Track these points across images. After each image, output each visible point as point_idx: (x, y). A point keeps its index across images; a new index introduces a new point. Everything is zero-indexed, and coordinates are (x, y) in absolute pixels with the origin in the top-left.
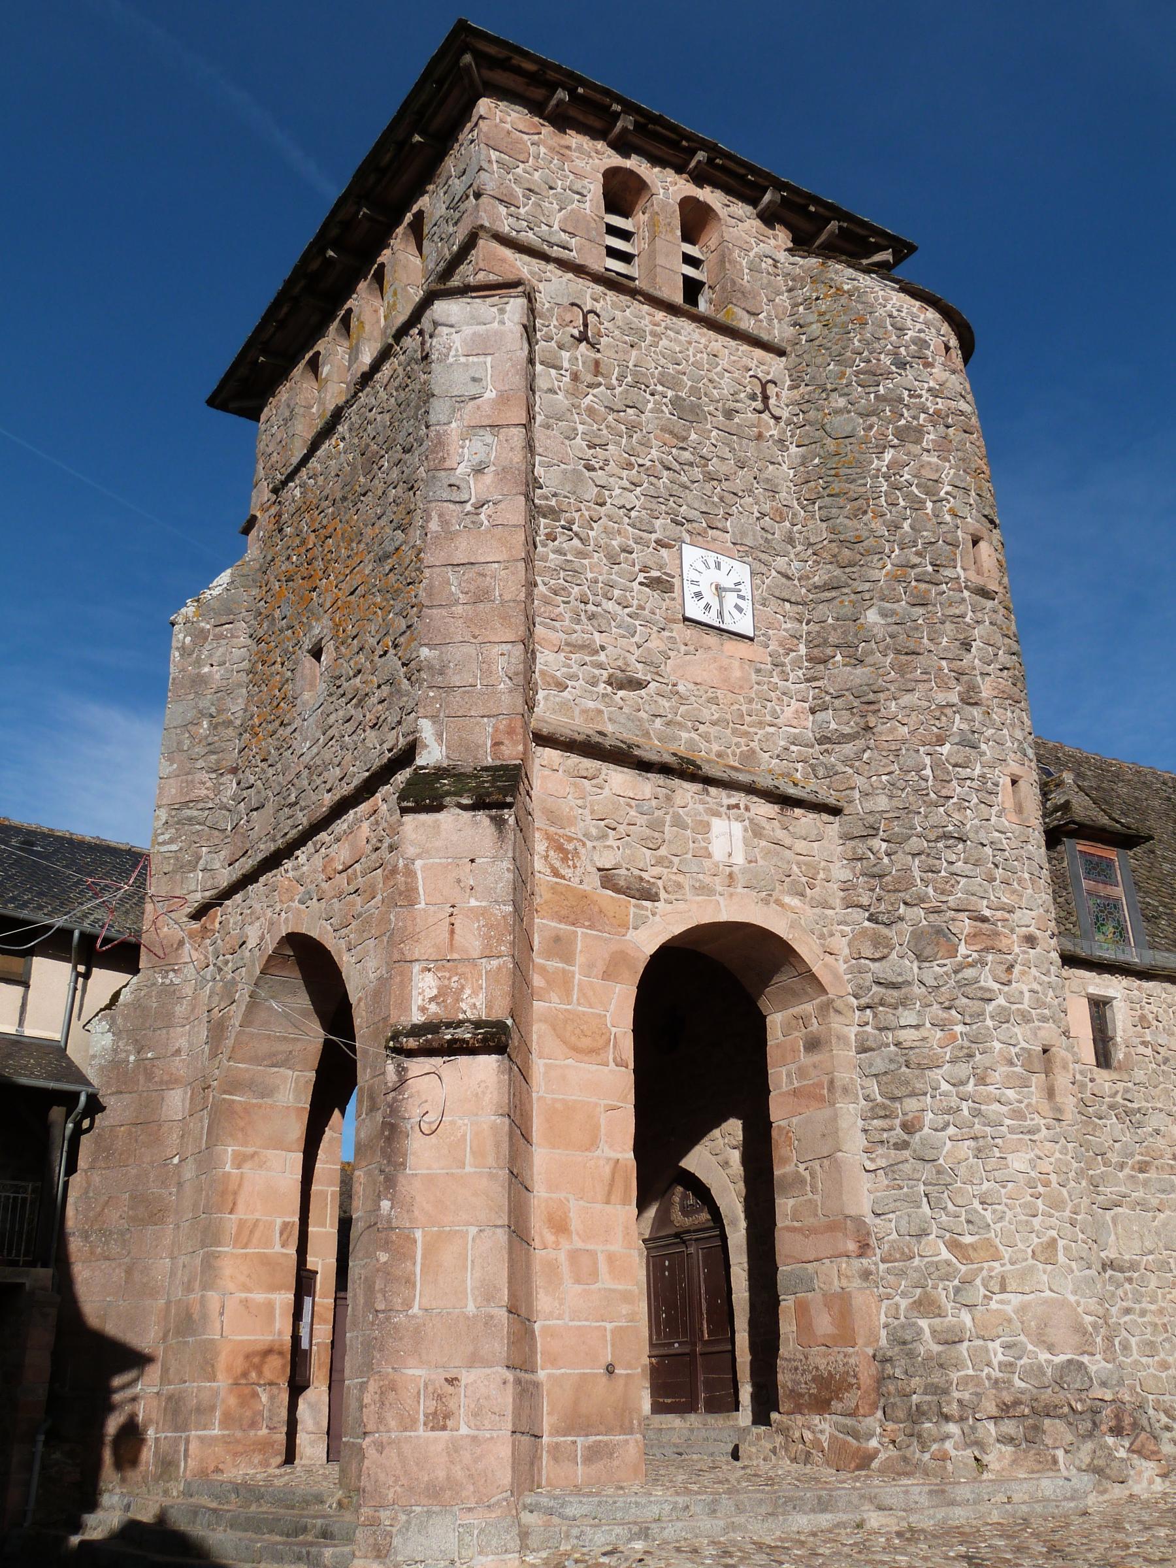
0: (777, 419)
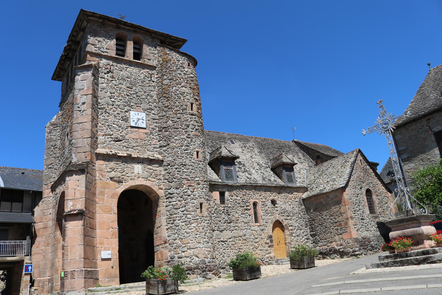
0: (154, 82)
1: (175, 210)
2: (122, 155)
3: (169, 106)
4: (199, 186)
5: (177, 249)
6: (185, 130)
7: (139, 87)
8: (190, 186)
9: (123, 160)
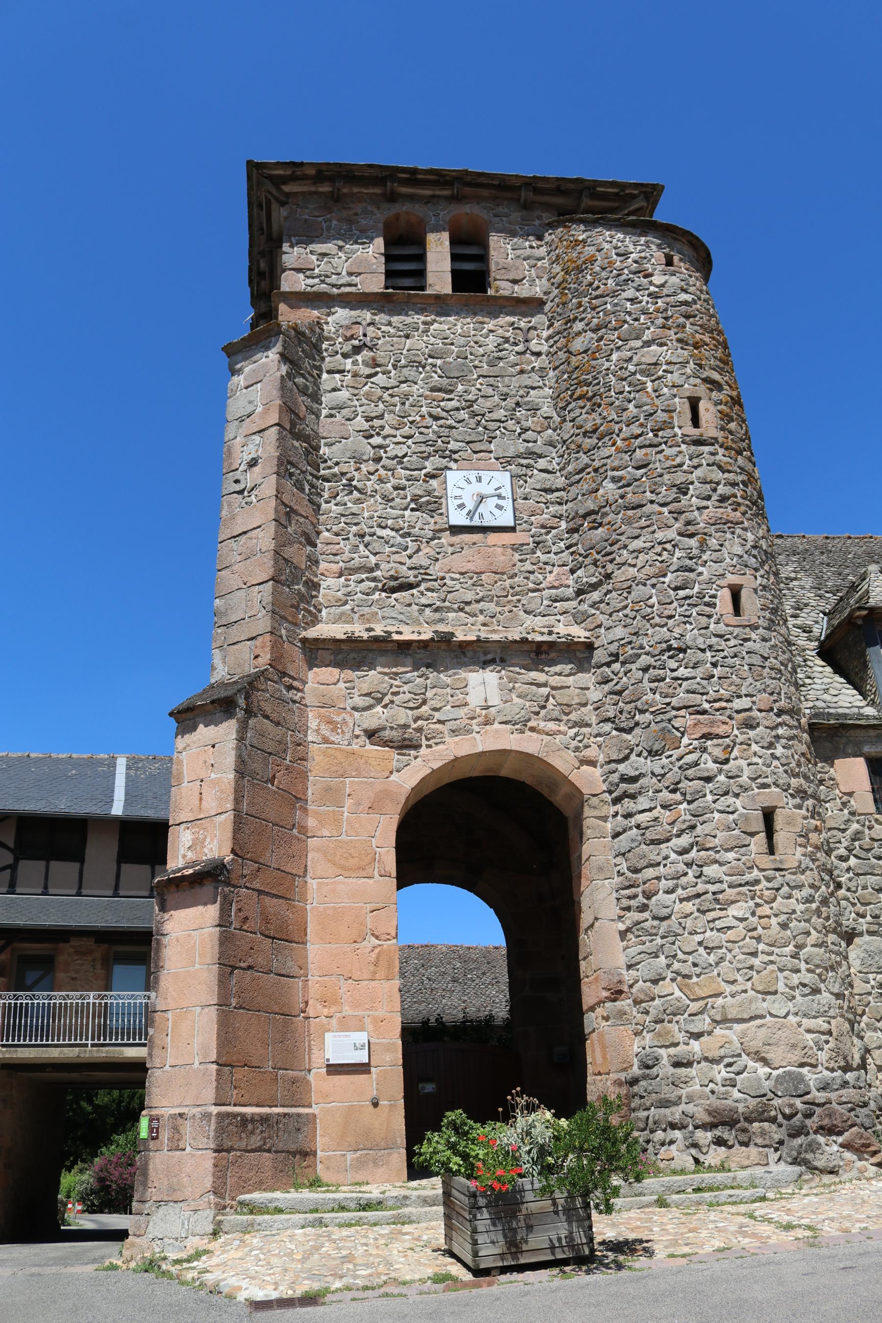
0: (538, 354)
2: (415, 637)
3: (602, 428)
4: (752, 733)
5: (666, 1023)
6: (670, 507)
7: (480, 380)
8: (707, 736)
9: (418, 656)
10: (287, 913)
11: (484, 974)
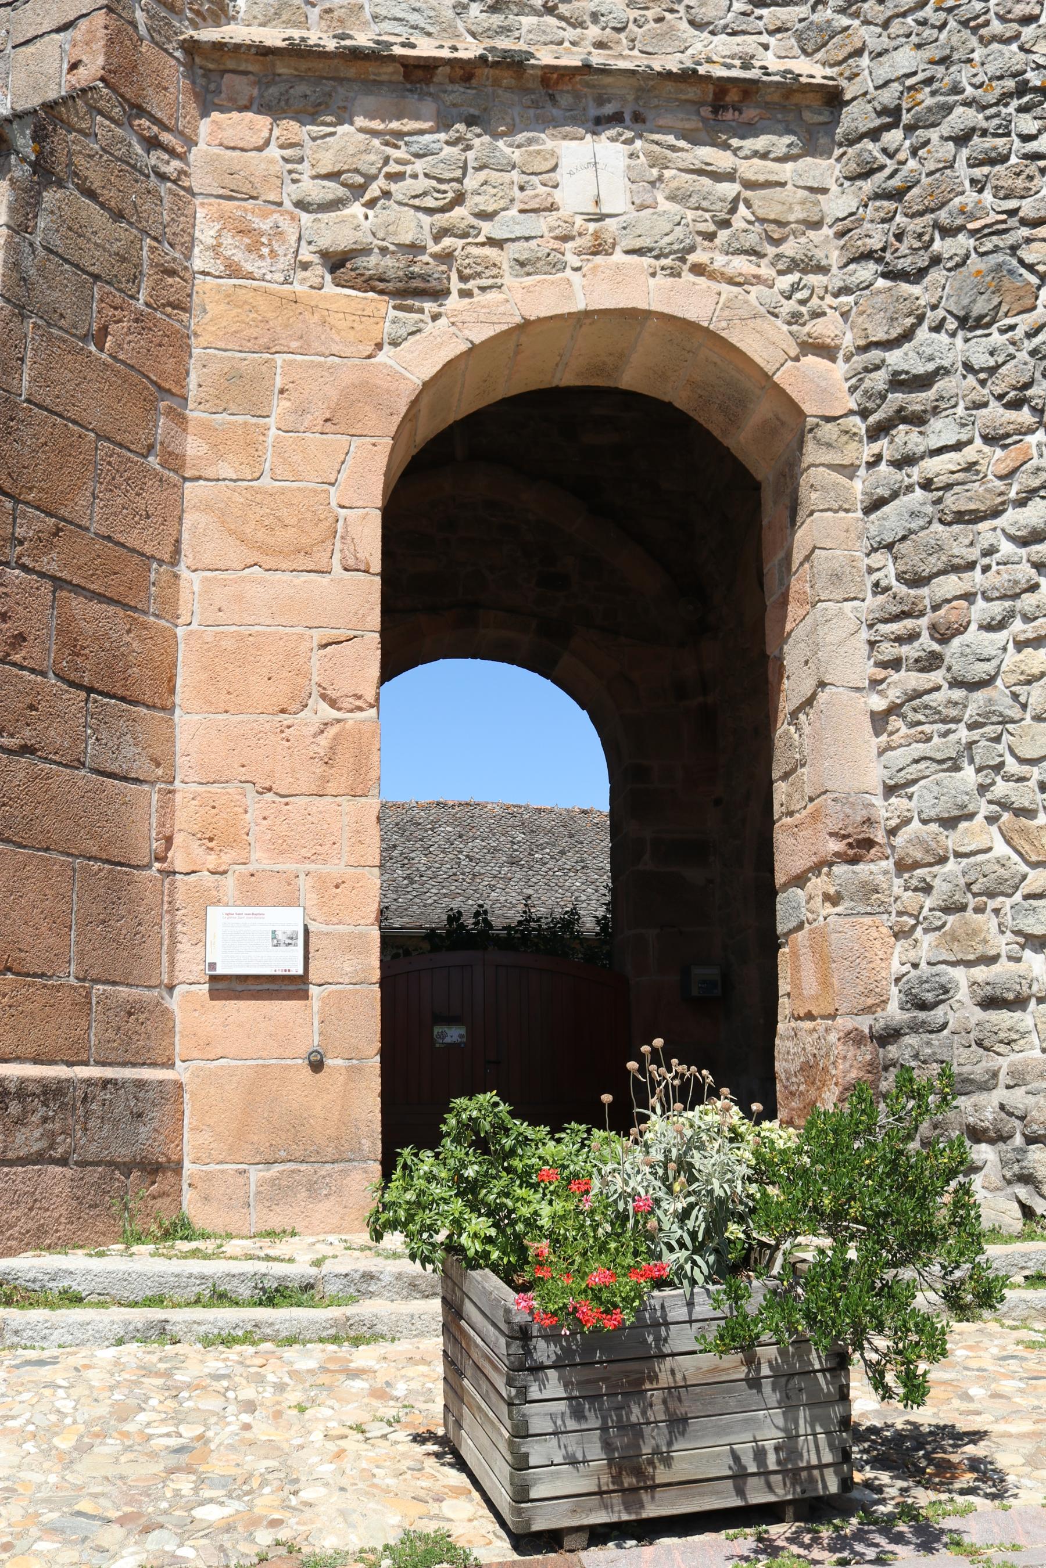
1: (956, 528)
2: (445, 53)
5: (969, 913)
9: (449, 99)
10: (127, 638)
11: (562, 853)
